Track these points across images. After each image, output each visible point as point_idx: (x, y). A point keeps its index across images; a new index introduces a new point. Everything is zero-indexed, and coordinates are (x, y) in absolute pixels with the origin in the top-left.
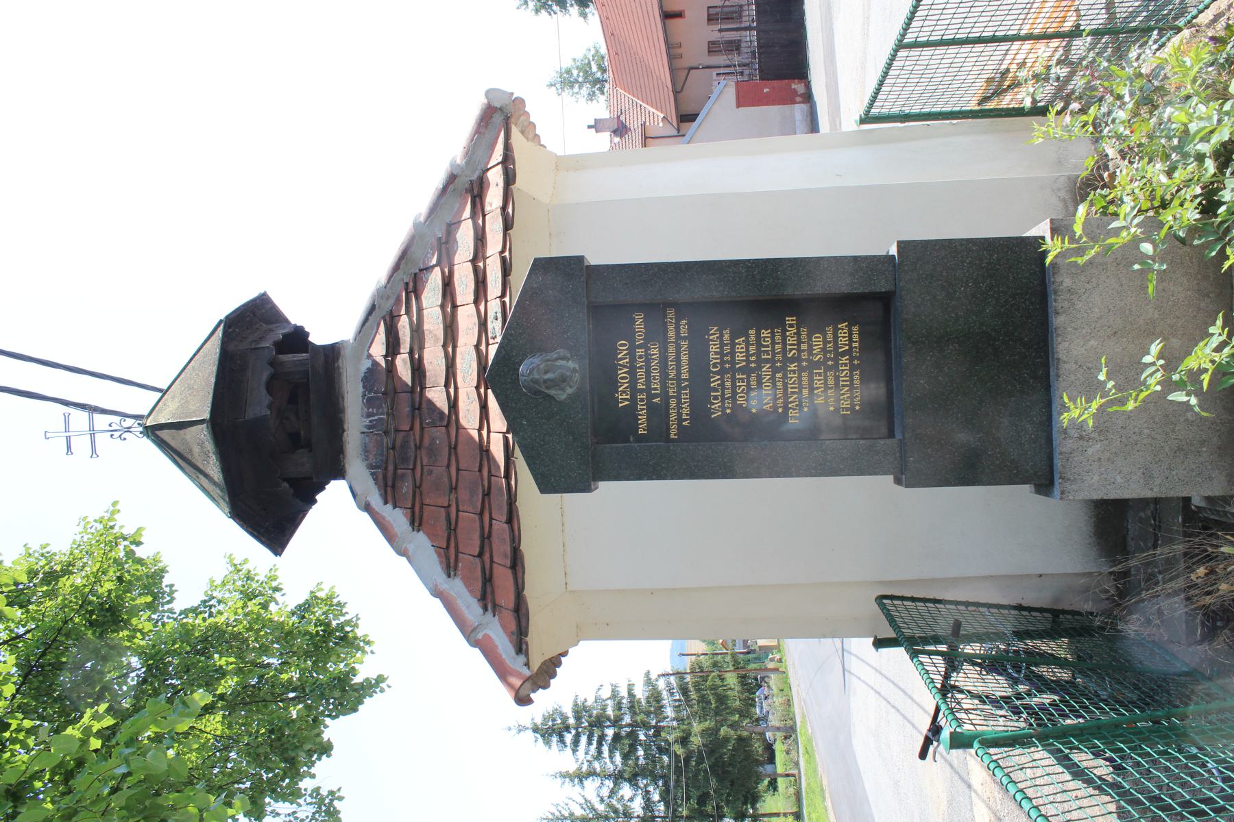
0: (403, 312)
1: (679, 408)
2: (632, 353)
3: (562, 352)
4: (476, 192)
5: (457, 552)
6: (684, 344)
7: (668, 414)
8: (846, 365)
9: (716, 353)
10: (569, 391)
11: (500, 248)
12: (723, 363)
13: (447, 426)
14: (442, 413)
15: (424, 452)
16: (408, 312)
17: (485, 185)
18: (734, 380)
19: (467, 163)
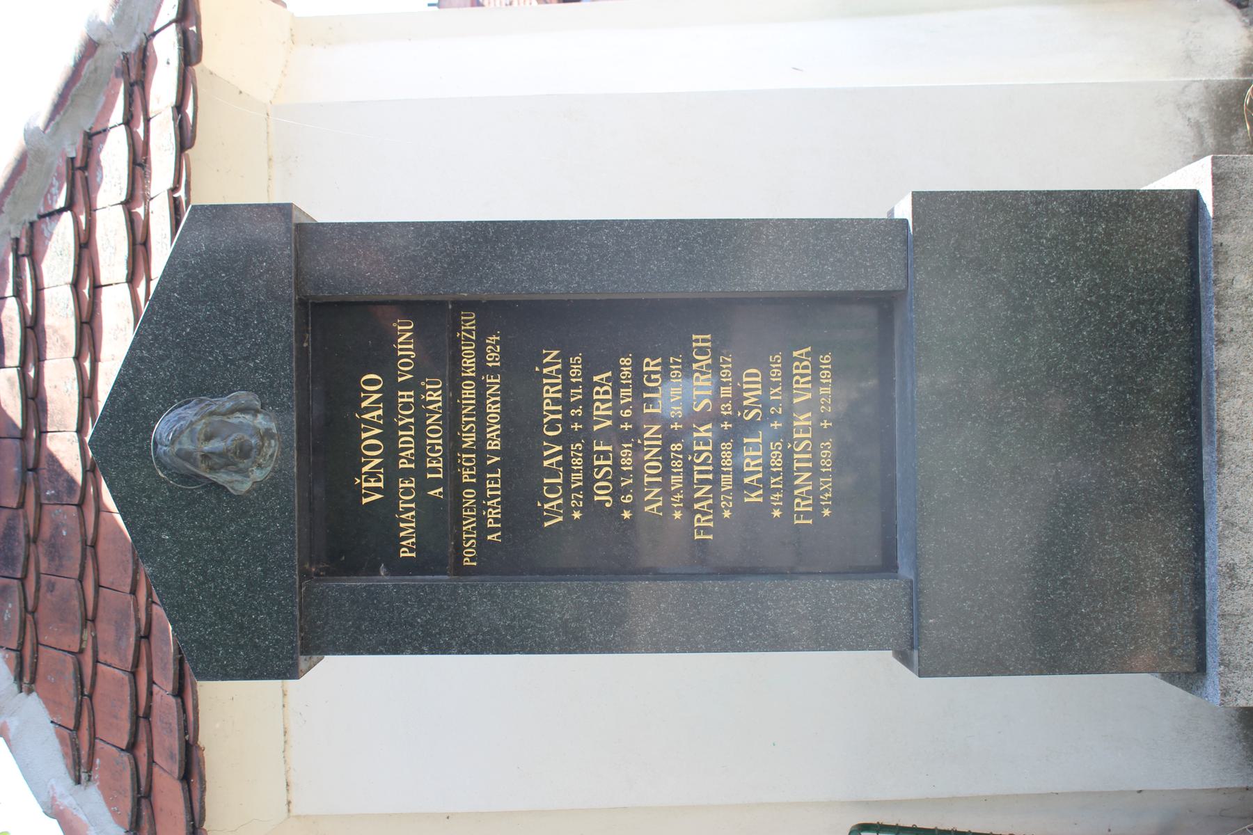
0: (9, 291)
1: (481, 506)
2: (389, 400)
3: (244, 397)
4: (133, 76)
5: (93, 737)
6: (494, 383)
7: (459, 520)
8: (806, 430)
9: (555, 401)
10: (258, 475)
11: (170, 184)
12: (567, 420)
13: (80, 505)
14: (71, 481)
15: (42, 549)
16: (18, 293)
17: (150, 64)
18: (588, 454)
19: (118, 20)
